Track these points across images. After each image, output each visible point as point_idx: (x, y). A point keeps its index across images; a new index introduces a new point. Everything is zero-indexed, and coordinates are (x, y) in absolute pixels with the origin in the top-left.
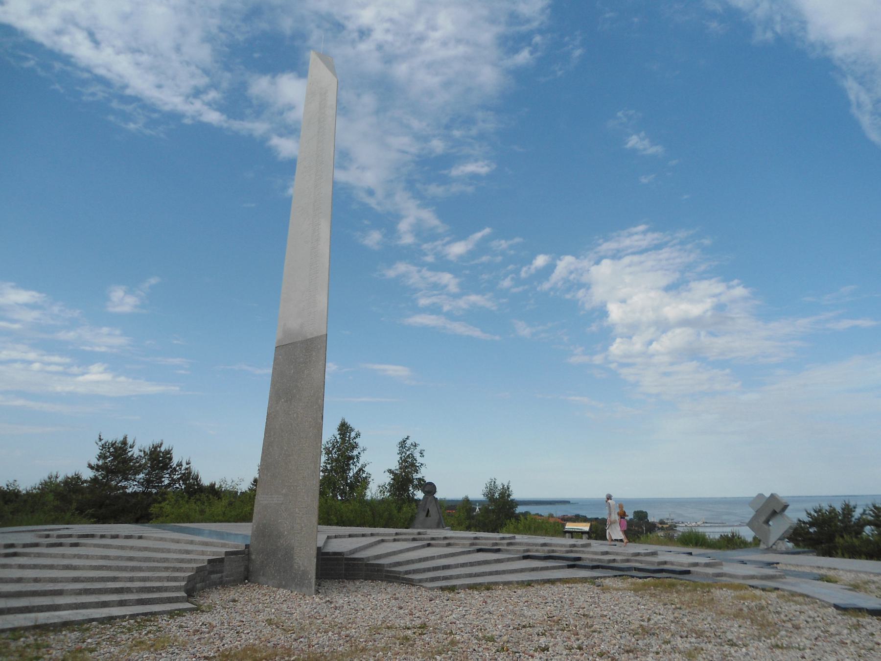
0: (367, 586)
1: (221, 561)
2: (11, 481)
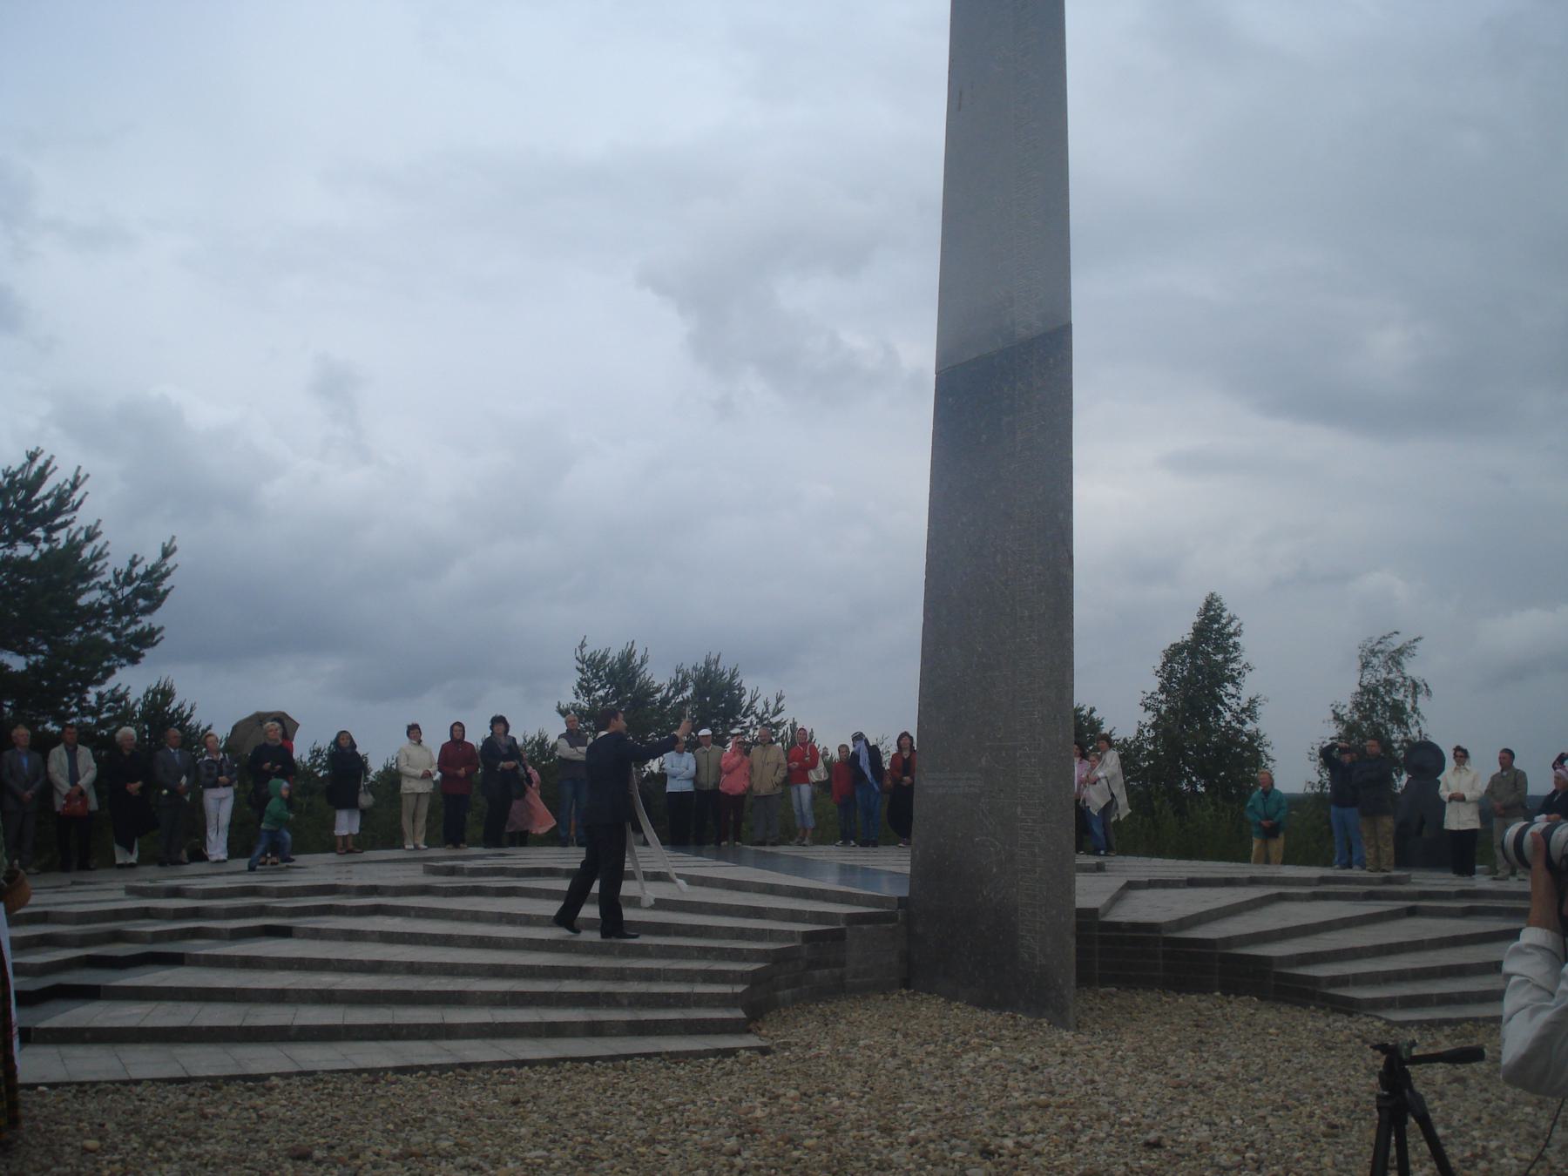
0: (1241, 1009)
1: (837, 936)
2: (1359, 652)
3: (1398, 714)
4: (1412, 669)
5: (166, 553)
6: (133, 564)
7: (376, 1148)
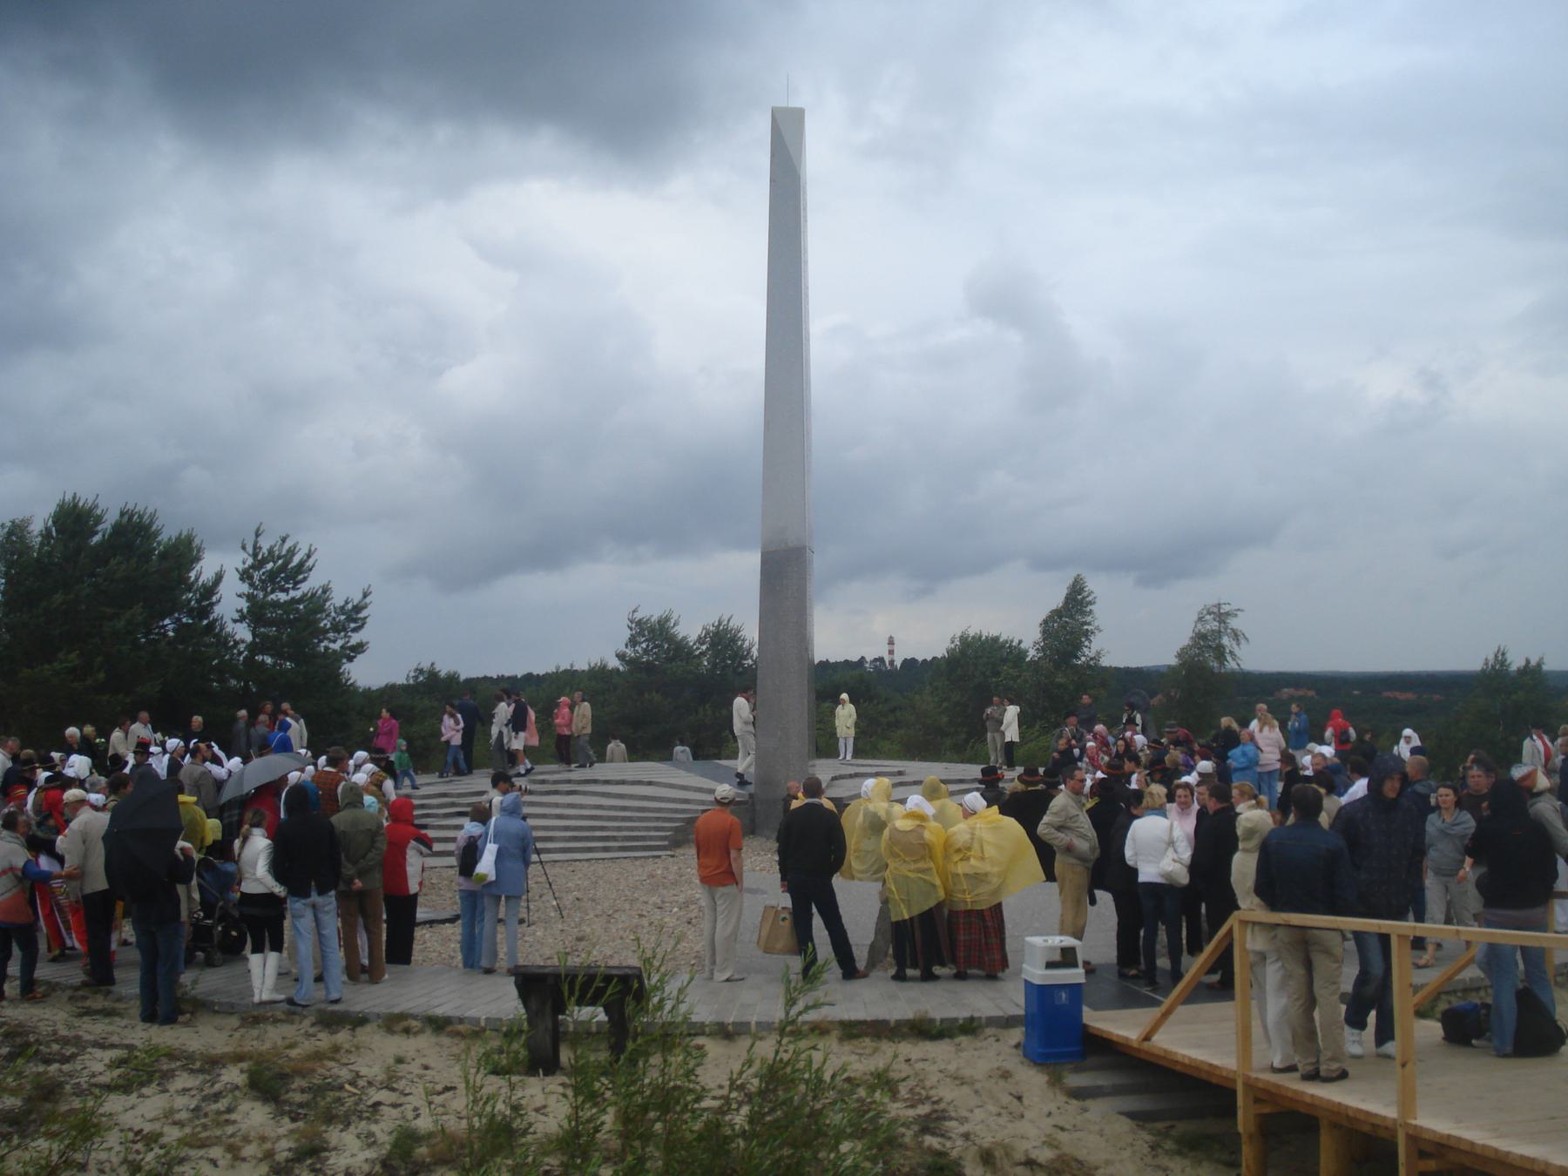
3: (1220, 653)
4: (1233, 623)
5: (365, 595)
6: (347, 603)
7: (424, 1061)
